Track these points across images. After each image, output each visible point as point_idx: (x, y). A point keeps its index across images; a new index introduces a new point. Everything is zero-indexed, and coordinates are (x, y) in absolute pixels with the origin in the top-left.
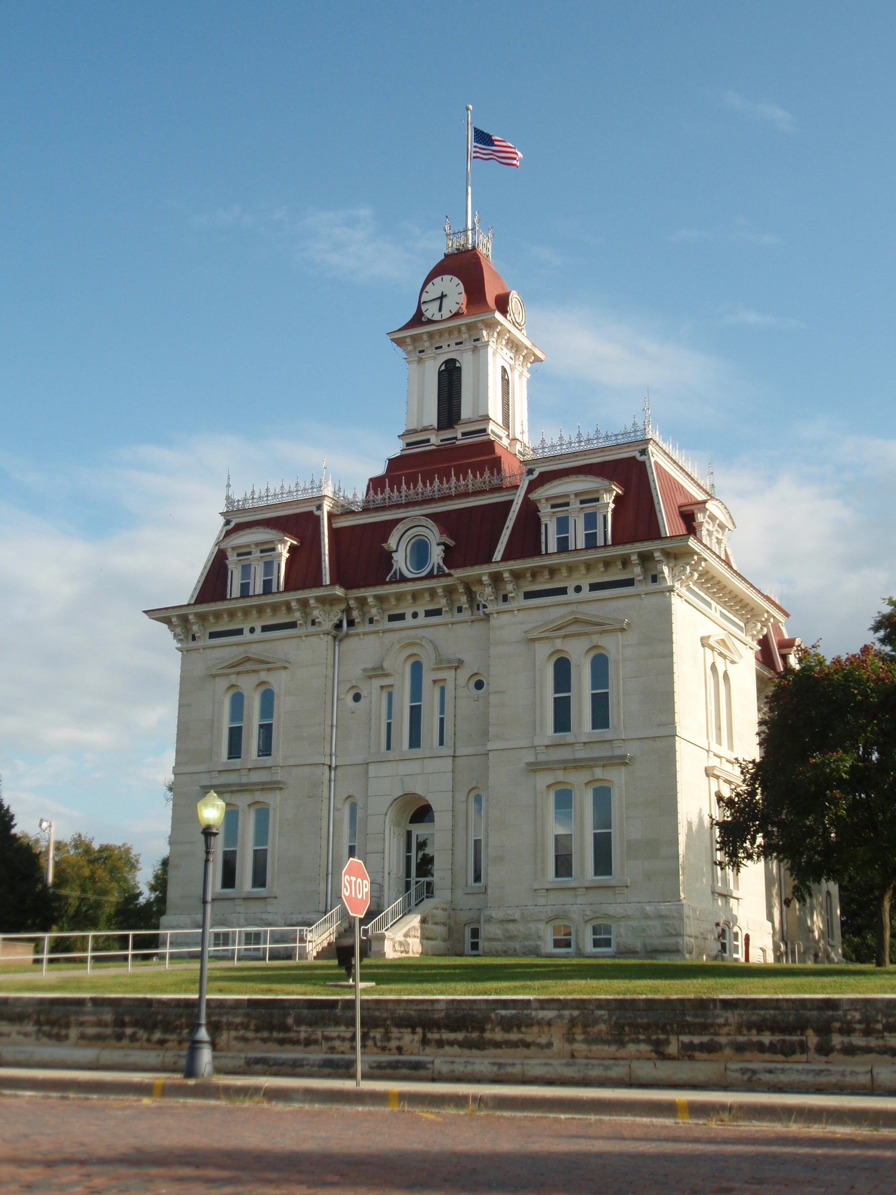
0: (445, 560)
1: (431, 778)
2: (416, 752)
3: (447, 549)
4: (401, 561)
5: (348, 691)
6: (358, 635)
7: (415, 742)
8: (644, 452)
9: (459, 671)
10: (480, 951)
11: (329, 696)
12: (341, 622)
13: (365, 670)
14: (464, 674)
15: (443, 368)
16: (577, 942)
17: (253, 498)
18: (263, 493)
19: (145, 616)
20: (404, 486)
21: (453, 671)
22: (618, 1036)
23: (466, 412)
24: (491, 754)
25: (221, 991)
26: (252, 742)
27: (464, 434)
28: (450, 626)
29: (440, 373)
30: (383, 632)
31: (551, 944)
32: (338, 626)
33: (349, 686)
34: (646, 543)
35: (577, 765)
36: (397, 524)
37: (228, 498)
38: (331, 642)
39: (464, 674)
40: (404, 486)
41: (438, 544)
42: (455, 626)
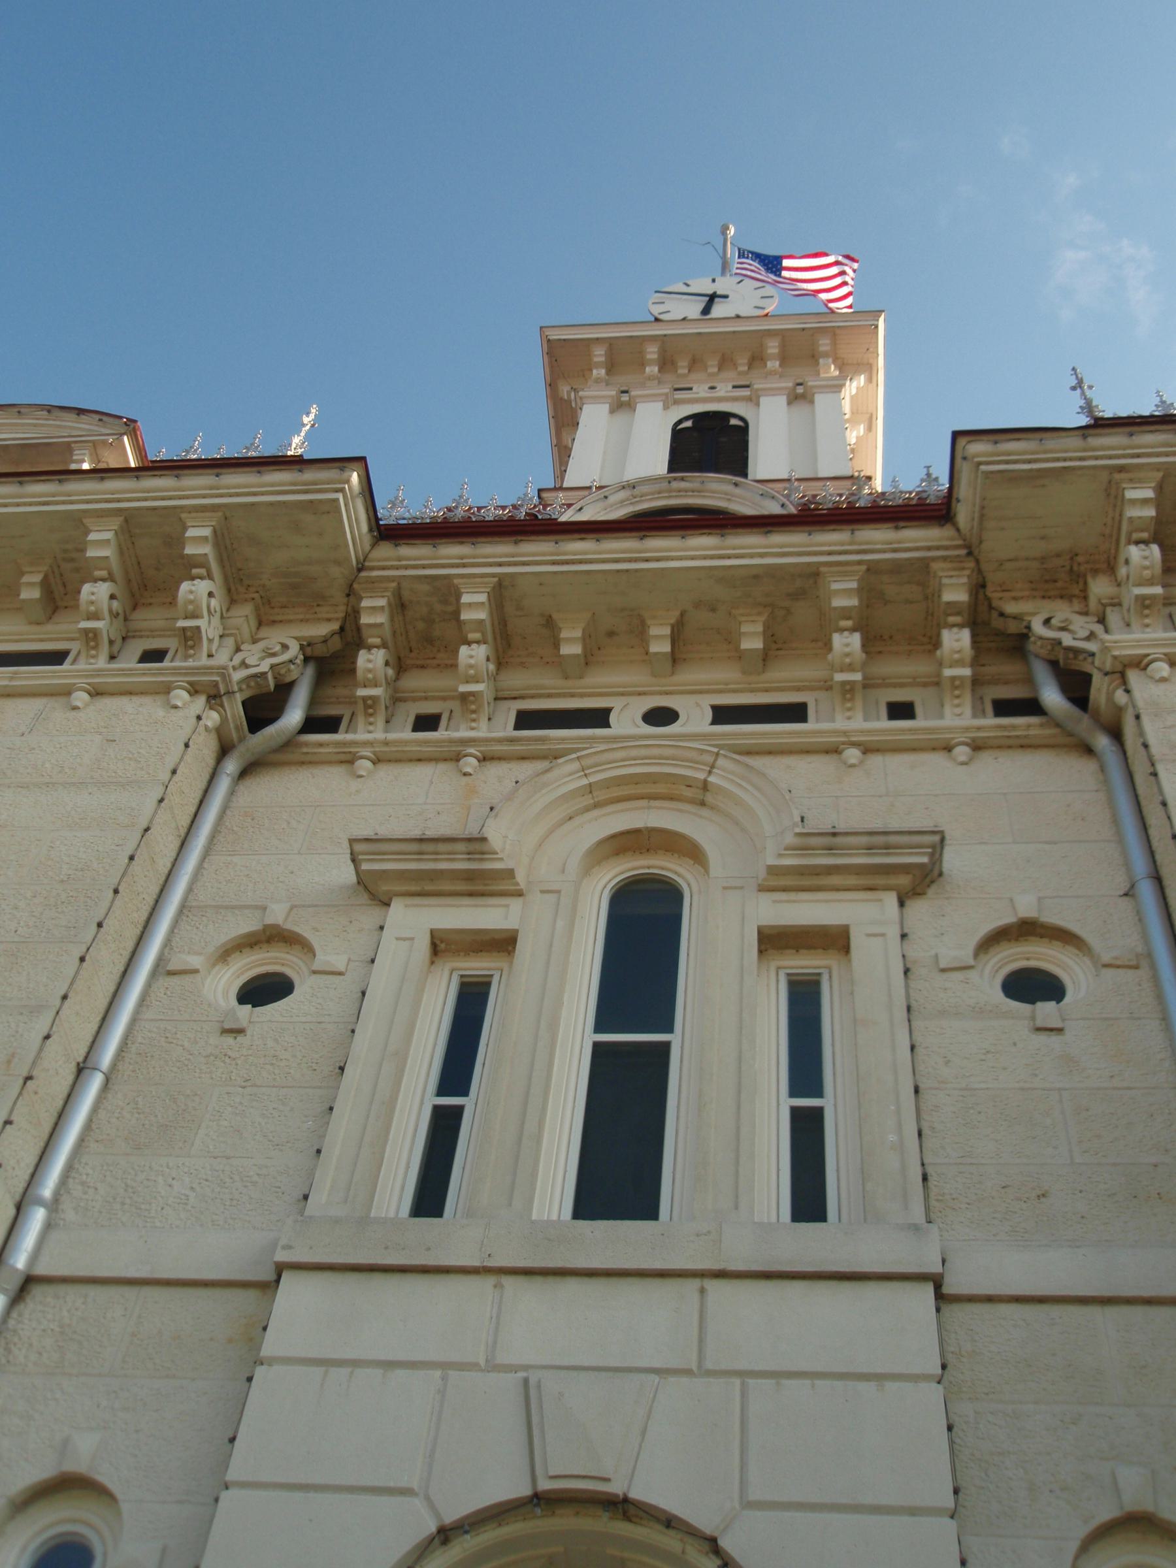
2: (616, 1240)
5: (226, 954)
7: (621, 1168)
11: (108, 959)
12: (284, 690)
13: (358, 847)
14: (948, 928)
15: (689, 424)
21: (891, 899)
25: (1014, 727)
28: (853, 754)
30: (484, 759)
32: (262, 709)
33: (248, 924)
36: (767, 257)
38: (206, 747)
39: (948, 928)
42: (876, 760)
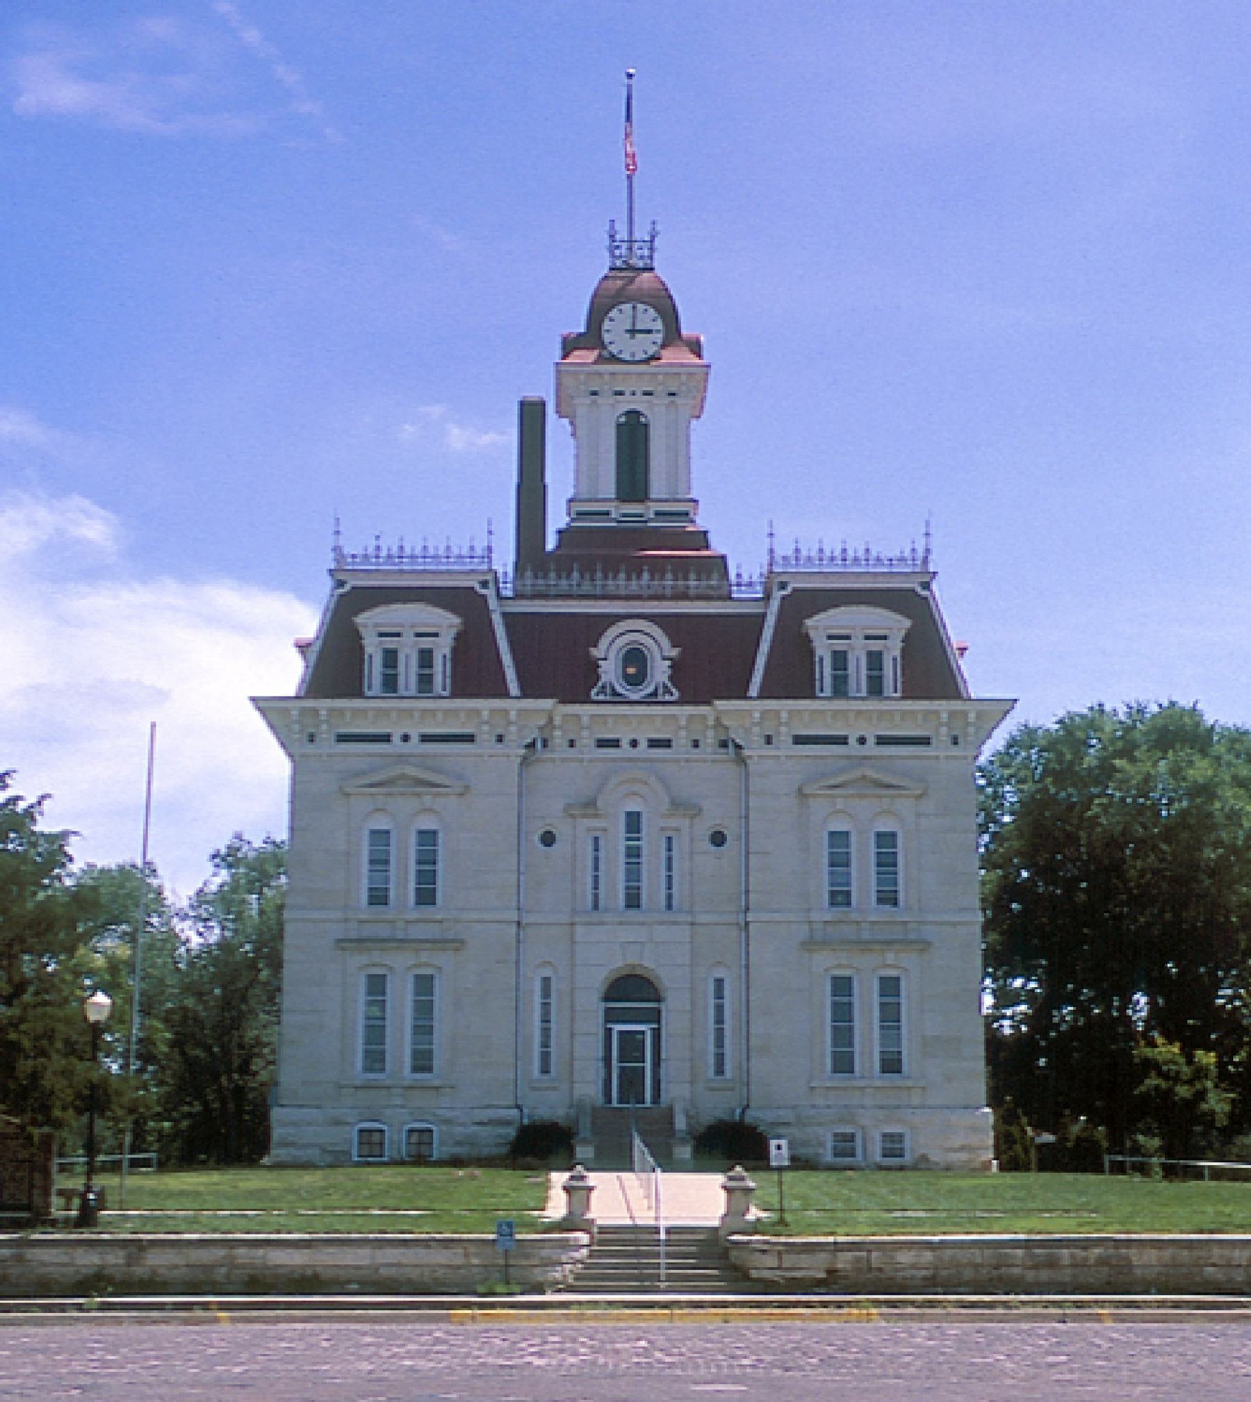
0: (671, 678)
1: (659, 948)
3: (676, 666)
4: (610, 671)
6: (553, 760)
8: (926, 586)
9: (697, 820)
10: (908, 1159)
16: (865, 1149)
17: (377, 557)
18: (395, 551)
19: (250, 707)
20: (599, 575)
22: (165, 1283)
23: (658, 487)
24: (149, 858)
26: (403, 886)
27: (658, 514)
29: (619, 426)
31: (829, 1151)
34: (885, 684)
35: (864, 946)
37: (337, 549)
40: (599, 575)
41: (664, 659)
